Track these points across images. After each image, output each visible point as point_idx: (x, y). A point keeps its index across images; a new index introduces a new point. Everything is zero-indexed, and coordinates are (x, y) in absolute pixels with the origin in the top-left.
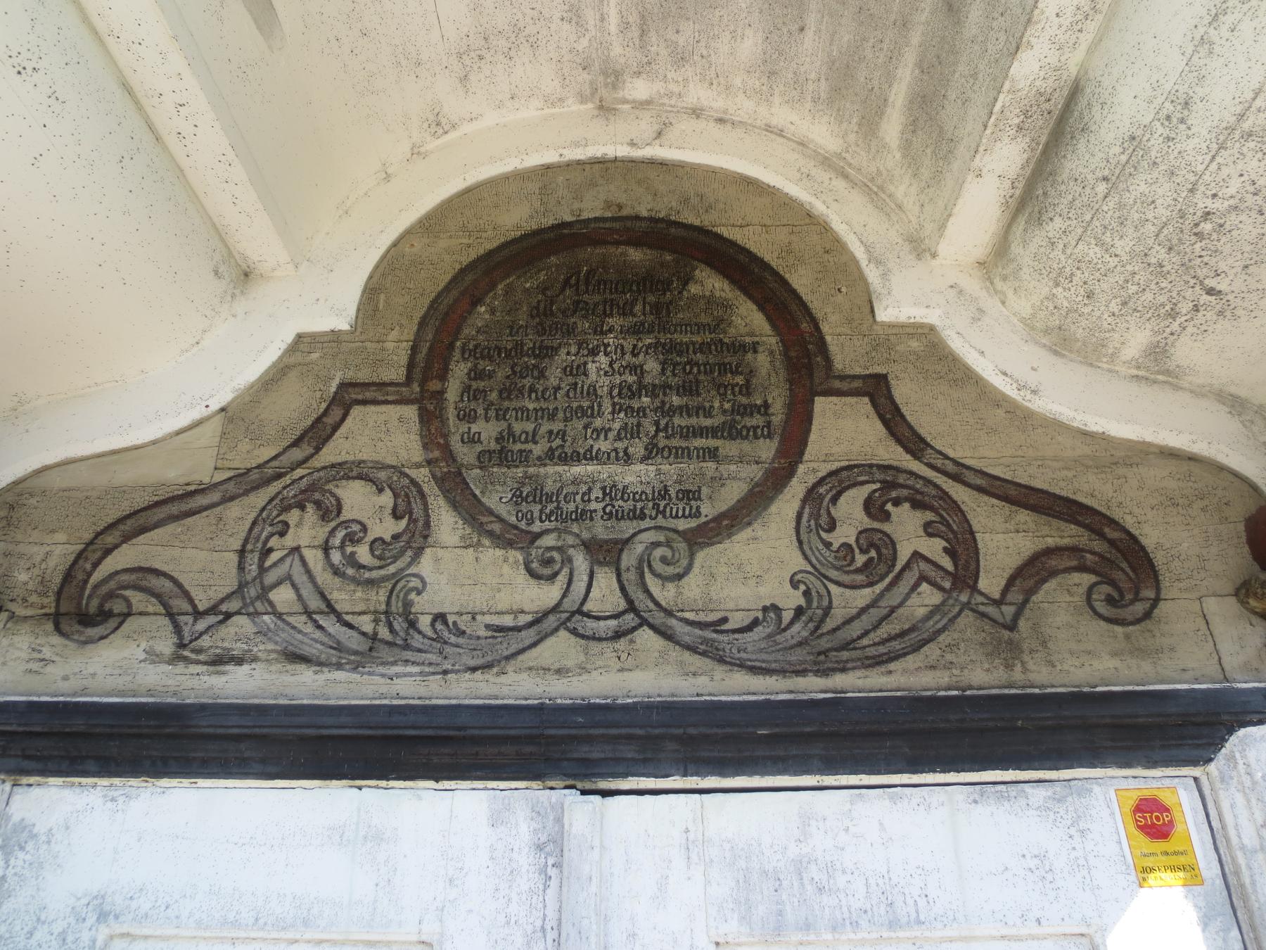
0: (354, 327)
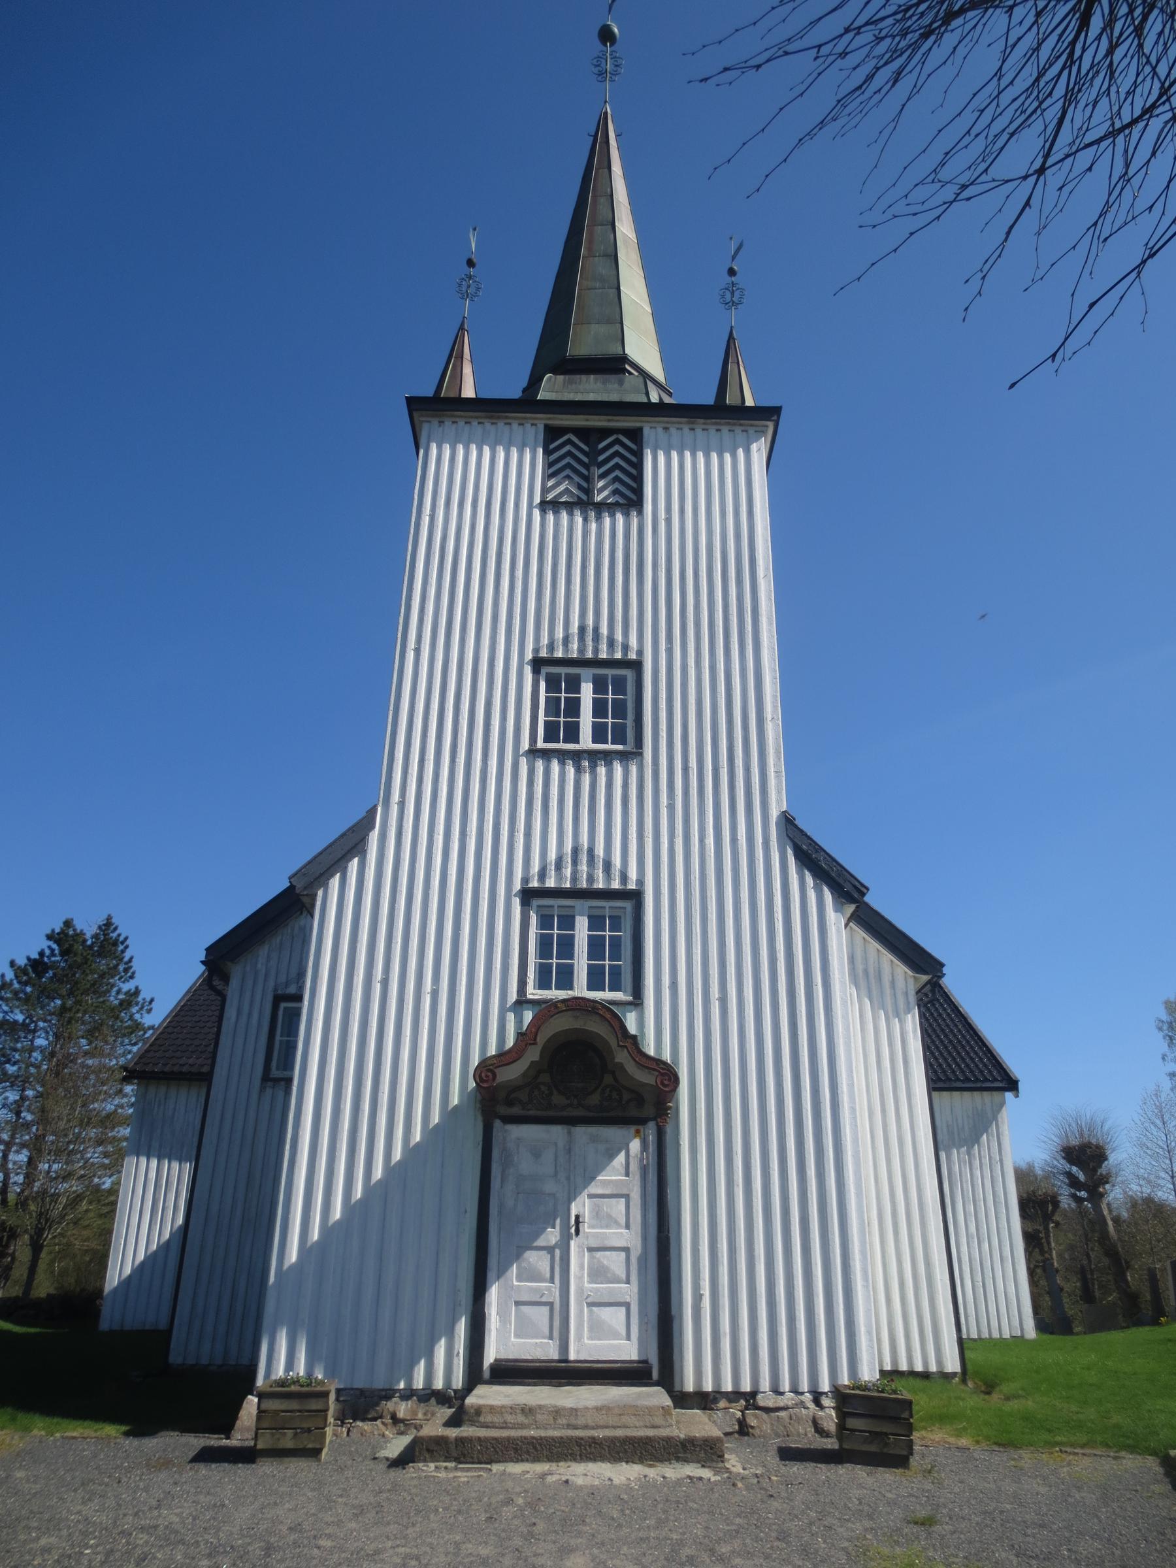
0: (245, 1397)
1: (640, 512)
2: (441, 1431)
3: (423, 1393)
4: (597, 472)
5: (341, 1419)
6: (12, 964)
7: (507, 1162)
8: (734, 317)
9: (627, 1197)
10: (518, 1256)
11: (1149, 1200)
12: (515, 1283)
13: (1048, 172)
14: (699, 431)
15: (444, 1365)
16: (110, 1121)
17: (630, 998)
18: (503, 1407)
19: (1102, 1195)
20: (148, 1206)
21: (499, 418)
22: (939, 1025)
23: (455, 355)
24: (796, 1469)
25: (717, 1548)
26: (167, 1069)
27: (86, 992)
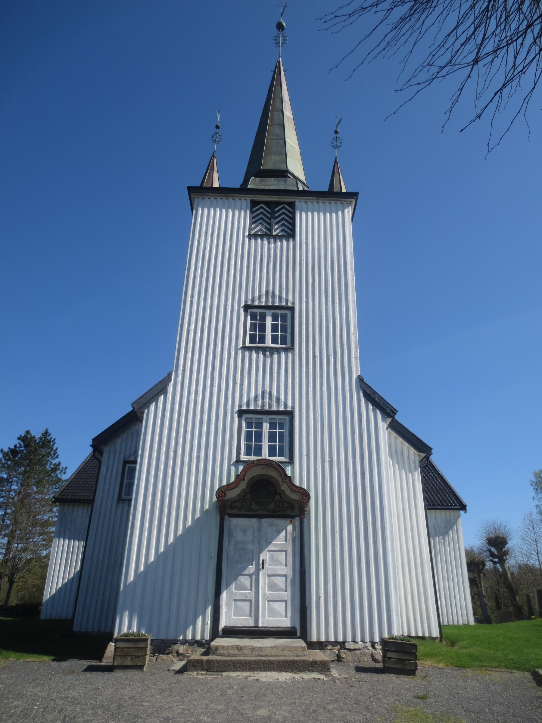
0: (109, 643)
1: (294, 240)
2: (200, 657)
3: (191, 641)
4: (274, 221)
5: (153, 653)
6: (2, 451)
7: (230, 535)
8: (337, 152)
9: (286, 551)
10: (235, 579)
11: (527, 566)
12: (234, 591)
13: (481, 64)
14: (321, 203)
15: (201, 628)
16: (46, 524)
17: (288, 460)
18: (228, 646)
19: (505, 561)
20: (63, 563)
21: (230, 196)
22: (430, 480)
23: (210, 168)
24: (363, 675)
25: (327, 707)
26: (73, 498)
27: (35, 464)
